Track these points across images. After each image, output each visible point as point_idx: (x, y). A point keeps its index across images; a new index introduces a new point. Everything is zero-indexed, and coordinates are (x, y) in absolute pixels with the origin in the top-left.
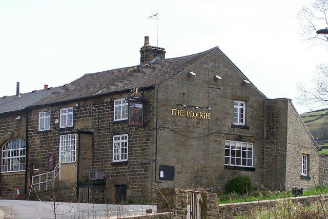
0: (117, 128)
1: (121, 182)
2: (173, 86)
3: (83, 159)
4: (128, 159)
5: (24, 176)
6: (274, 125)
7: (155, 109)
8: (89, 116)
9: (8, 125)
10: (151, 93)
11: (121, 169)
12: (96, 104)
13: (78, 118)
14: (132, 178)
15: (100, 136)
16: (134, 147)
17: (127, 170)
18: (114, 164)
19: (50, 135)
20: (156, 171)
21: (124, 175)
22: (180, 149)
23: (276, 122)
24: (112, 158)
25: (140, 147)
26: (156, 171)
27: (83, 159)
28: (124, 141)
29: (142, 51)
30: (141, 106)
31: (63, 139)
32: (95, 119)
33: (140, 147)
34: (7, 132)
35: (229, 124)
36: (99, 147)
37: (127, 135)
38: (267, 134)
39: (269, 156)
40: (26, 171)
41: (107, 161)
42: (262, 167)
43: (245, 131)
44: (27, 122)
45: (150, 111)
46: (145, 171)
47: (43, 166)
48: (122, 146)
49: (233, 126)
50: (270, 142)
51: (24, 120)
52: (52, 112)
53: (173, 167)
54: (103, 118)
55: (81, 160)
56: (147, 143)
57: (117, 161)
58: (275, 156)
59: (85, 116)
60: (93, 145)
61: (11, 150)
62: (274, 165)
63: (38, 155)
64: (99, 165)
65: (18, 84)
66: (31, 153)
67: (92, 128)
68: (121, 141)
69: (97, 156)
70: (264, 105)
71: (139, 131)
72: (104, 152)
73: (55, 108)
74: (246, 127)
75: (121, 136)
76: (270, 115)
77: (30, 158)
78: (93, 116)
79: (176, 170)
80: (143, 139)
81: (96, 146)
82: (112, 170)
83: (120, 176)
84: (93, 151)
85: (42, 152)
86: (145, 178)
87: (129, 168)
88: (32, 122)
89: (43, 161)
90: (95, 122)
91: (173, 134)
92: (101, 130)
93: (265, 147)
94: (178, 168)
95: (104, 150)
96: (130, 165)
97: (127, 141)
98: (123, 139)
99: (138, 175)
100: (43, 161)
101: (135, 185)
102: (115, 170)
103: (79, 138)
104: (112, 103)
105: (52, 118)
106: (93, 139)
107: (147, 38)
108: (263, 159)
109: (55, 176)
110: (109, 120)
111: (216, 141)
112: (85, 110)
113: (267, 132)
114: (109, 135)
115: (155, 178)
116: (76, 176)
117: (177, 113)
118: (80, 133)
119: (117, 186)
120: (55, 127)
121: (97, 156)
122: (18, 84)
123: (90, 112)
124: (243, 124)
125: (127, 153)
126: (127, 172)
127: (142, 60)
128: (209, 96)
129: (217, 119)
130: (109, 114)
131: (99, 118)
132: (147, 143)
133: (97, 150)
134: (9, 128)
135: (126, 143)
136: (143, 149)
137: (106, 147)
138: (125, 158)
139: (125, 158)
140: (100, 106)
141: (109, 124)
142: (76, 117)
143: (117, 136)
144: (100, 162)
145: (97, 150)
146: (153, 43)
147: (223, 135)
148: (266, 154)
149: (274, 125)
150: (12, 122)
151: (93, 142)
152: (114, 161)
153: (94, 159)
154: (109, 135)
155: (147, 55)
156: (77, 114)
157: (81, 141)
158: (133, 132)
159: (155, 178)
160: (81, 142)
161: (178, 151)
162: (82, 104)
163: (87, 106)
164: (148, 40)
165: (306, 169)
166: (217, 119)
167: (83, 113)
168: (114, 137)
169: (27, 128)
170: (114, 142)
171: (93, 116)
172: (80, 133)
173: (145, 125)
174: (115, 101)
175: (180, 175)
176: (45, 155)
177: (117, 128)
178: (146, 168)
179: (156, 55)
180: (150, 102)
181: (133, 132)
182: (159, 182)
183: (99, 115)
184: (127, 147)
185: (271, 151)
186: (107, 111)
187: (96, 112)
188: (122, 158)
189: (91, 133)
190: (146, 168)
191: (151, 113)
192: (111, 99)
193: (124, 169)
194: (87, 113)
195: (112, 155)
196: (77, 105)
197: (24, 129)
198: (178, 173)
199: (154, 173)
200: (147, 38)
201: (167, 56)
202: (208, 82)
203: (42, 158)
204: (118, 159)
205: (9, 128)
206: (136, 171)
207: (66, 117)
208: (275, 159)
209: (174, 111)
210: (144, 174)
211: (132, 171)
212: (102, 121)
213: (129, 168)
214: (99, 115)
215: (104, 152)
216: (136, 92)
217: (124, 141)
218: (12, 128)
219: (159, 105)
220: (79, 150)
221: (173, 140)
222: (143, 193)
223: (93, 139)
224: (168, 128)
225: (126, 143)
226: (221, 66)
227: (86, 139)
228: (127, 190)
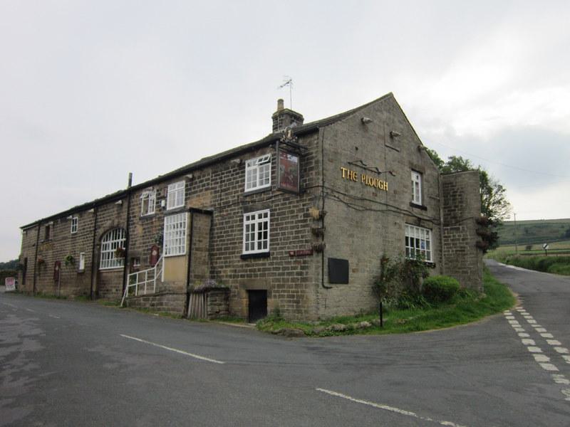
0: (249, 202)
1: (258, 285)
2: (343, 133)
3: (197, 249)
4: (270, 249)
5: (122, 274)
6: (456, 207)
7: (320, 164)
8: (207, 190)
9: (108, 213)
10: (314, 139)
11: (257, 265)
12: (217, 172)
13: (190, 194)
14: (278, 280)
15: (223, 216)
16: (282, 229)
17: (267, 266)
18: (244, 258)
19: (154, 220)
20: (323, 269)
21: (264, 275)
22: (355, 232)
23: (461, 202)
24: (242, 248)
25: (292, 228)
26: (323, 269)
27: (197, 249)
28: (263, 220)
29: (275, 118)
30: (295, 159)
31: (168, 222)
32: (216, 192)
33: (292, 228)
34: (107, 220)
35: (408, 201)
36: (221, 233)
37: (268, 211)
38: (445, 219)
39: (450, 248)
40: (125, 268)
41: (234, 253)
42: (441, 262)
43: (424, 212)
44: (129, 207)
45: (312, 169)
46: (303, 268)
47: (145, 260)
48: (260, 229)
49: (412, 205)
50: (451, 229)
51: (126, 205)
52: (158, 191)
53: (347, 261)
54: (229, 189)
55: (194, 251)
56: (305, 221)
57: (250, 252)
58: (461, 247)
59: (201, 191)
60: (211, 230)
61: (111, 241)
62: (460, 260)
63: (139, 247)
64: (220, 258)
65: (131, 175)
66: (132, 245)
67: (212, 206)
68: (257, 221)
69: (217, 245)
70: (439, 183)
71: (290, 203)
72: (228, 240)
73: (162, 185)
74: (423, 208)
75: (256, 214)
76: (449, 193)
77: (130, 251)
78: (212, 188)
79: (352, 266)
80: (297, 216)
81: (216, 231)
82: (242, 266)
83: (256, 276)
84: (211, 238)
85: (144, 243)
86: (305, 280)
87: (272, 264)
88: (134, 206)
89: (145, 254)
90: (216, 197)
91: (346, 209)
92: (225, 207)
93: (443, 235)
94: (352, 263)
95: (228, 236)
96: (274, 258)
97: (268, 219)
98: (260, 217)
99: (289, 274)
100: (145, 254)
101: (284, 291)
102: (247, 266)
103: (192, 218)
104: (241, 166)
105: (158, 199)
106: (212, 221)
107: (281, 102)
108: (441, 251)
109: (157, 273)
110: (237, 192)
111: (396, 223)
112: (201, 181)
113: (444, 215)
114: (238, 213)
115: (323, 280)
116: (186, 276)
117: (350, 176)
118: (193, 211)
119: (250, 292)
120: (162, 210)
121: (217, 245)
122: (131, 175)
123: (208, 184)
124: (420, 203)
125: (268, 240)
126: (269, 269)
127: (275, 128)
128: (385, 158)
129: (395, 192)
130: (237, 182)
131: (222, 191)
132: (305, 221)
133: (218, 237)
134: (109, 216)
135: (266, 223)
136: (297, 232)
137: (232, 231)
138: (265, 247)
139: (265, 247)
140: (223, 174)
141: (238, 197)
142: (189, 193)
143: (250, 214)
144: (222, 254)
145: (218, 237)
146: (287, 106)
147: (402, 215)
148: (445, 244)
149: (456, 207)
150: (113, 208)
151: (212, 225)
152: (245, 252)
153: (214, 250)
154: (238, 213)
155: (282, 120)
156: (190, 189)
157: (195, 223)
158: (278, 205)
159: (323, 280)
160: (195, 225)
161: (351, 236)
162: (197, 174)
163: (204, 176)
164: (273, 126)
165: (101, 260)
166: (395, 192)
167: (199, 187)
168: (245, 215)
169: (129, 214)
170: (246, 223)
171: (212, 188)
172: (193, 211)
173: (303, 192)
174: (247, 162)
175: (355, 275)
176: (147, 246)
177: (249, 202)
178: (305, 262)
179: (293, 121)
180: (312, 153)
181: (278, 205)
182: (327, 288)
183: (221, 186)
184: (268, 230)
185: (453, 240)
186: (234, 179)
187: (218, 183)
188: (259, 248)
189: (210, 213)
190: (305, 262)
191: (314, 172)
192: (241, 161)
193: (264, 264)
194: (204, 186)
195: (242, 242)
196: (190, 176)
197: (125, 215)
198: (354, 271)
199: (321, 272)
200: (281, 102)
201: (305, 122)
202: (383, 138)
203: (144, 250)
204: (253, 249)
205: (109, 216)
206: (284, 269)
207: (176, 191)
208: (460, 251)
209: (346, 172)
210: (301, 274)
211: (278, 269)
212: (226, 194)
213: (272, 264)
214: (221, 186)
215: (228, 240)
216: (289, 135)
217: (263, 220)
218: (112, 215)
219: (326, 159)
220: (191, 236)
221: (346, 218)
222: (297, 307)
223: (212, 221)
224: (338, 198)
225: (266, 223)
226: (396, 119)
227: (202, 222)
228: (269, 300)
